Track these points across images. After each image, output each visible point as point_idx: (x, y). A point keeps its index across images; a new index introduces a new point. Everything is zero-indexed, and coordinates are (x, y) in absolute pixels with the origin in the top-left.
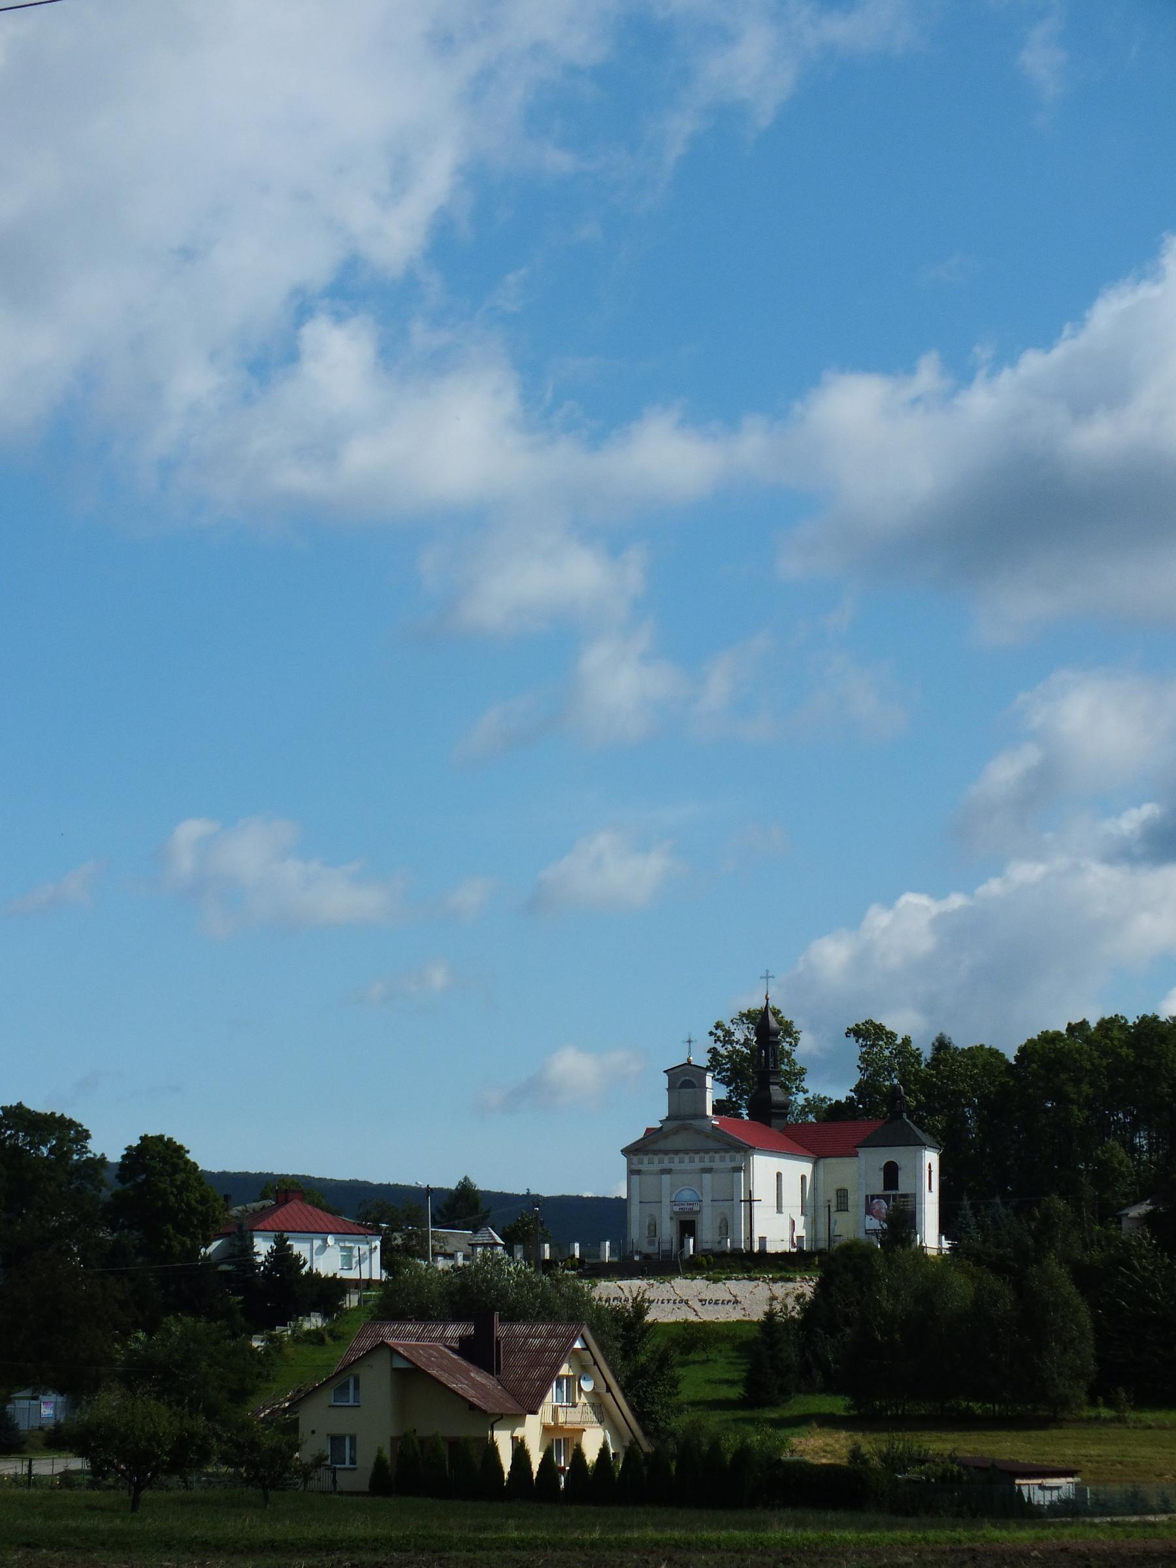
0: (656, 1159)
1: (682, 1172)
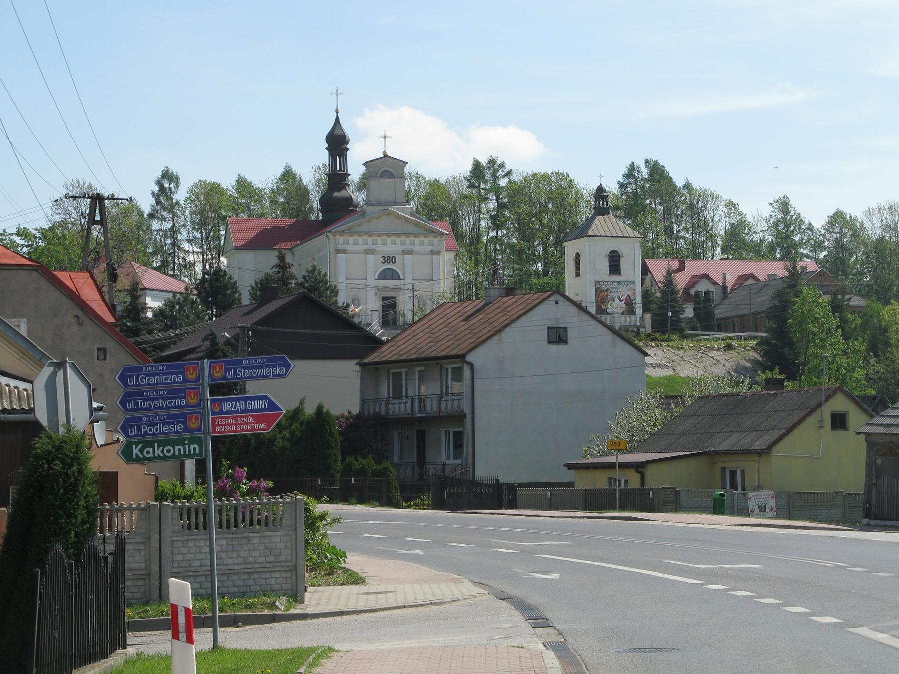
0: (361, 240)
1: (419, 253)
